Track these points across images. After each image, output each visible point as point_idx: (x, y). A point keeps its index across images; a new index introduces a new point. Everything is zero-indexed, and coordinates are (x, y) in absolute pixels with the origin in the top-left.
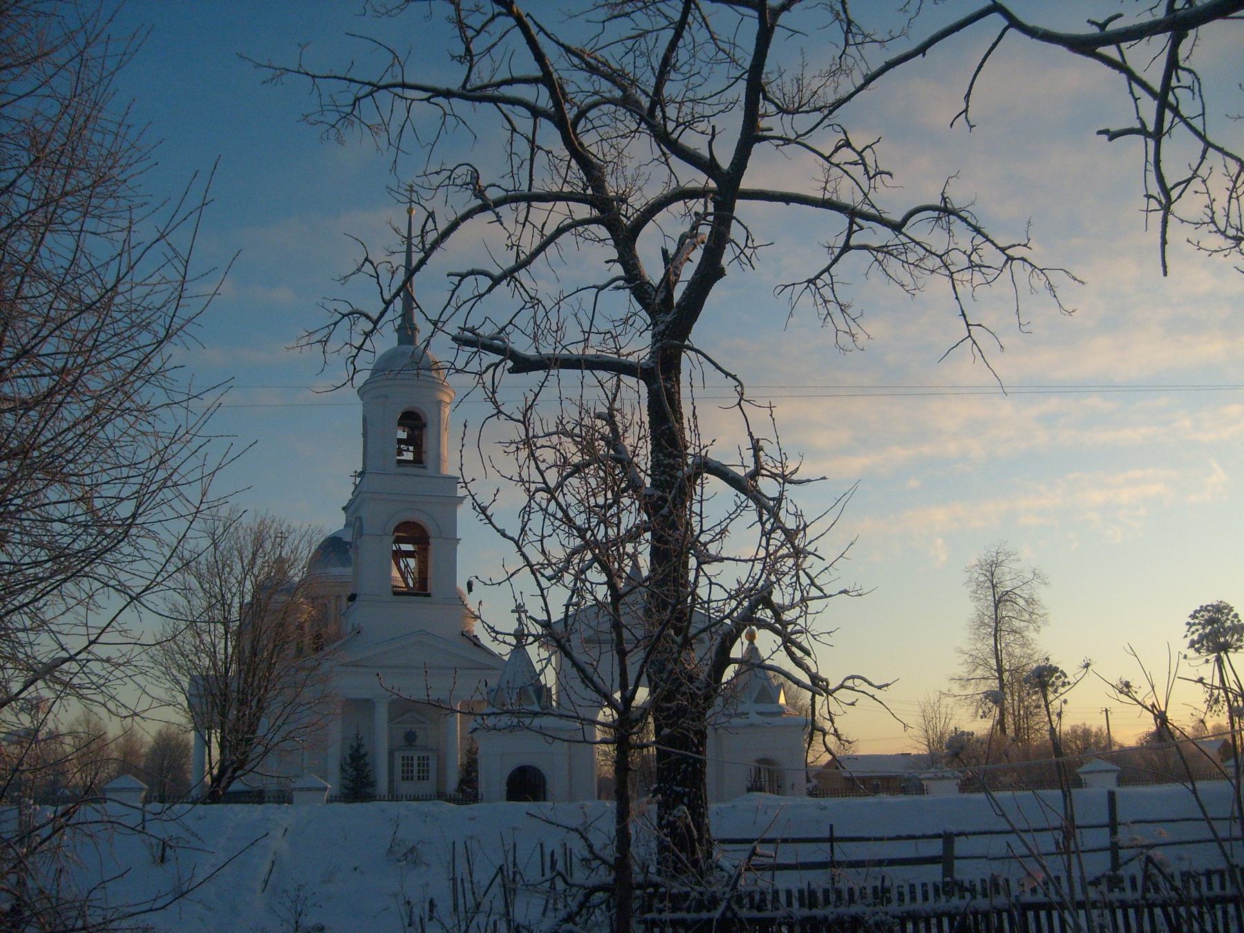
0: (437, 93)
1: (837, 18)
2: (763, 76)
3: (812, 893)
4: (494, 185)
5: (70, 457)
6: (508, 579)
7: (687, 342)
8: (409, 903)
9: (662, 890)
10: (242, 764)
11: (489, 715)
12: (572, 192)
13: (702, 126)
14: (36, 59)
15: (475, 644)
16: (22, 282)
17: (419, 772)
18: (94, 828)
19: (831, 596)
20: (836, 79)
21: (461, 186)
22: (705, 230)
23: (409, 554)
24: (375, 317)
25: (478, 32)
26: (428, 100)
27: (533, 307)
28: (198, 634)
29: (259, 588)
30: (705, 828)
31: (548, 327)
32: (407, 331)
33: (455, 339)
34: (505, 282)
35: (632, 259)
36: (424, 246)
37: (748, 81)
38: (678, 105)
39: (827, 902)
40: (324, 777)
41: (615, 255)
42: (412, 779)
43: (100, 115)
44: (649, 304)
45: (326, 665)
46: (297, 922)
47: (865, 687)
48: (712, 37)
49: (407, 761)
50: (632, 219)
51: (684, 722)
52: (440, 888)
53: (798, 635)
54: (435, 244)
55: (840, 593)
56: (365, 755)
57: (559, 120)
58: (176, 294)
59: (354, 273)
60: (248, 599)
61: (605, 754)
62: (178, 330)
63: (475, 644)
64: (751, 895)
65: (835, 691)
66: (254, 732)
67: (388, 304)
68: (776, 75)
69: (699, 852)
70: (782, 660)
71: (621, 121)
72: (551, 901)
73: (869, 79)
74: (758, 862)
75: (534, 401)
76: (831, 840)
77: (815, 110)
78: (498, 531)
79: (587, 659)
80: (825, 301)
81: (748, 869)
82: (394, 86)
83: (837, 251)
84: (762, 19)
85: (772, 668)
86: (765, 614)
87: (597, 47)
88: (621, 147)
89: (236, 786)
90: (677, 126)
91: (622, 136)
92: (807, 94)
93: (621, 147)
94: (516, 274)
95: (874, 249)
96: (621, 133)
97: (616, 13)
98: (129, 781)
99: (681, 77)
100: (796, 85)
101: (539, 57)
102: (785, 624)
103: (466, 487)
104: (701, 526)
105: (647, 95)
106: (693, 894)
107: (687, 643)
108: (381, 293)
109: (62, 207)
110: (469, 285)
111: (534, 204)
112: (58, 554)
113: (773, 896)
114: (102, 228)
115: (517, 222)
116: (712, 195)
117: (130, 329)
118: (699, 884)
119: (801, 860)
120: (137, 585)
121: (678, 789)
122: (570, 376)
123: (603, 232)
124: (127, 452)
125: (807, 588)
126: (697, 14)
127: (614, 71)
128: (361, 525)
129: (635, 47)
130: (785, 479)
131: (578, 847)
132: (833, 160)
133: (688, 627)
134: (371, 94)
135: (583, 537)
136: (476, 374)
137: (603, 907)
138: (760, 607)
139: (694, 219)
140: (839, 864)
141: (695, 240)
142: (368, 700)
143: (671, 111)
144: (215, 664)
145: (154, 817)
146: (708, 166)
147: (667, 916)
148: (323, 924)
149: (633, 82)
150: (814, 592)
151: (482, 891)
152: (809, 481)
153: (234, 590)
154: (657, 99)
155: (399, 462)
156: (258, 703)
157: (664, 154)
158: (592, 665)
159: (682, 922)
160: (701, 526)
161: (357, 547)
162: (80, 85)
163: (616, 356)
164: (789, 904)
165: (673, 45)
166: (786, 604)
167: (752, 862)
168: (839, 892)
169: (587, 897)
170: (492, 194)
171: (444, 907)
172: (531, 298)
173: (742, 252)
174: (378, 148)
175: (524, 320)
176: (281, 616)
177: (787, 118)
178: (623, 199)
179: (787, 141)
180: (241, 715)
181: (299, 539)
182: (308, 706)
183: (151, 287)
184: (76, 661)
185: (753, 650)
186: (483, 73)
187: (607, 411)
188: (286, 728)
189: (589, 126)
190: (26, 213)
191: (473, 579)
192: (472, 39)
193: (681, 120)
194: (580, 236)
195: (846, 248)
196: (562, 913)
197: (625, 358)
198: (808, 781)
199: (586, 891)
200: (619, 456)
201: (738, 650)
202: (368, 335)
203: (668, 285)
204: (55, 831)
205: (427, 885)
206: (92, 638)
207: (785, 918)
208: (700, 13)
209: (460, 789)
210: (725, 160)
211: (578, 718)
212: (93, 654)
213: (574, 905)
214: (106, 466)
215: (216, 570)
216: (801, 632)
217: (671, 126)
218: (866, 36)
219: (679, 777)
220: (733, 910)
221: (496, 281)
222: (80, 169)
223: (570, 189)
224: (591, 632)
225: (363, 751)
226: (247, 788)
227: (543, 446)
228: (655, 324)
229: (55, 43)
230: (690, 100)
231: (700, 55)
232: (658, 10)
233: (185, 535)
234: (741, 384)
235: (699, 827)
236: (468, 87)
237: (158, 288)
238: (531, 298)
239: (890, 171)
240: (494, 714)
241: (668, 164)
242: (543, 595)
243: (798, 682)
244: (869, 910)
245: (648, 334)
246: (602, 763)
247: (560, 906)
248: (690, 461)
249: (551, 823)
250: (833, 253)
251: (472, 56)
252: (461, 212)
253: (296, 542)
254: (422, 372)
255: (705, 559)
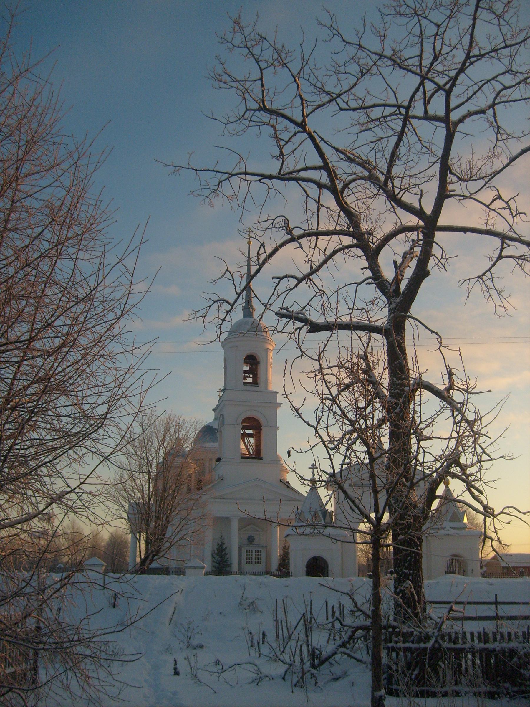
0: (265, 177)
1: (491, 125)
2: (449, 160)
3: (486, 634)
4: (297, 227)
5: (71, 381)
6: (311, 449)
7: (408, 314)
8: (251, 633)
9: (397, 630)
10: (158, 552)
11: (300, 526)
12: (341, 230)
13: (414, 190)
14: (53, 167)
15: (288, 487)
16: (45, 287)
17: (256, 559)
18: (83, 585)
19: (495, 459)
20: (491, 161)
21: (279, 228)
22: (418, 250)
23: (250, 435)
24: (232, 302)
25: (287, 142)
26: (259, 181)
27: (320, 295)
28: (134, 479)
29: (167, 454)
30: (422, 595)
31: (329, 306)
32: (248, 310)
33: (277, 314)
34: (304, 282)
35: (376, 267)
36: (259, 262)
37: (440, 163)
38: (400, 179)
39: (495, 640)
40: (203, 561)
41: (367, 265)
42: (252, 563)
43: (86, 196)
44: (387, 292)
45: (204, 498)
46: (188, 642)
47: (516, 513)
48: (419, 140)
49: (249, 553)
50: (376, 244)
51: (411, 532)
52: (269, 627)
53: (476, 482)
54: (265, 261)
55: (500, 458)
56: (226, 549)
57: (333, 190)
58: (128, 292)
59: (220, 278)
60: (161, 460)
61: (362, 550)
62: (128, 311)
63: (288, 487)
64: (449, 635)
65: (498, 515)
66: (164, 535)
67: (239, 295)
68: (457, 159)
69: (418, 608)
70: (467, 498)
71: (368, 189)
72: (332, 635)
73: (513, 159)
74: (454, 616)
75: (324, 348)
76: (496, 603)
77: (480, 178)
78: (305, 422)
79: (357, 496)
80: (488, 289)
81: (448, 619)
82: (241, 174)
83: (494, 260)
84: (448, 128)
85: (460, 501)
86: (456, 470)
87: (354, 148)
88: (369, 203)
89: (154, 565)
90: (401, 191)
91: (369, 197)
92: (475, 169)
93: (369, 203)
94: (310, 277)
95: (516, 258)
96: (368, 196)
97: (364, 128)
98: (96, 560)
99: (403, 163)
100: (468, 165)
101: (322, 155)
102: (467, 476)
103: (287, 397)
104: (421, 419)
105: (383, 174)
106: (415, 633)
107: (412, 485)
108: (235, 289)
109: (66, 246)
110: (284, 285)
111: (320, 237)
112: (66, 435)
113: (463, 636)
114: (87, 256)
115: (310, 247)
116: (421, 229)
117: (103, 311)
118: (419, 627)
119: (479, 614)
120: (107, 451)
121: (406, 571)
122: (344, 334)
123: (359, 252)
124: (101, 378)
125: (481, 454)
126: (410, 127)
127: (364, 161)
128: (223, 418)
129: (376, 147)
130: (467, 391)
131: (348, 603)
132: (491, 207)
133: (413, 477)
134: (228, 178)
135: (353, 425)
136: (289, 333)
137: (363, 639)
138: (453, 466)
139: (411, 243)
140: (502, 618)
141: (412, 255)
142: (227, 518)
143: (397, 183)
144: (143, 497)
145: (115, 580)
146: (419, 213)
147: (401, 645)
148: (203, 644)
149: (375, 167)
150: (485, 457)
151: (294, 627)
152: (481, 392)
153: (153, 455)
154: (389, 176)
155: (244, 383)
156: (166, 519)
157: (393, 207)
158: (358, 498)
159: (409, 649)
160: (421, 419)
161: (221, 432)
162: (75, 181)
163: (368, 322)
164: (472, 640)
165: (397, 145)
166: (468, 464)
167: (451, 615)
168: (502, 635)
169: (354, 632)
170: (297, 232)
171: (271, 637)
172: (319, 290)
173: (439, 261)
174: (232, 209)
175: (316, 303)
176: (179, 470)
177: (464, 184)
178: (370, 233)
179: (465, 197)
180: (157, 525)
181: (189, 426)
182: (194, 521)
183: (113, 288)
184: (75, 492)
185: (447, 490)
186: (290, 165)
187: (363, 354)
188: (182, 533)
189: (350, 192)
190: (48, 250)
191: (291, 449)
192: (283, 146)
193: (403, 187)
194: (346, 254)
195: (500, 257)
196: (339, 642)
197: (373, 323)
198: (481, 567)
199: (352, 629)
200: (370, 379)
201: (440, 490)
202: (228, 312)
203: (397, 280)
204: (62, 587)
205: (262, 623)
206: (82, 481)
207: (470, 649)
208: (412, 126)
209: (279, 570)
210: (428, 210)
211: (351, 529)
212: (83, 490)
213: (346, 638)
214: (90, 386)
215: (143, 444)
216: (477, 480)
217: (397, 191)
218: (508, 135)
219: (406, 564)
220: (439, 643)
221: (300, 281)
222: (76, 225)
223: (340, 228)
224: (357, 479)
225: (224, 547)
226: (160, 566)
227: (327, 374)
228: (390, 303)
229: (62, 159)
230: (408, 176)
231: (413, 150)
232: (388, 125)
233: (132, 424)
234: (440, 337)
235: (418, 593)
236: (282, 173)
237: (117, 289)
238: (319, 290)
239: (526, 212)
240: (302, 526)
241: (395, 213)
242: (330, 459)
243: (476, 510)
244: (520, 645)
245: (386, 310)
246: (360, 556)
247: (337, 637)
248: (412, 382)
249: (333, 589)
250: (492, 260)
251: (283, 156)
252: (279, 242)
253: (188, 429)
254: (259, 333)
255: (421, 438)
